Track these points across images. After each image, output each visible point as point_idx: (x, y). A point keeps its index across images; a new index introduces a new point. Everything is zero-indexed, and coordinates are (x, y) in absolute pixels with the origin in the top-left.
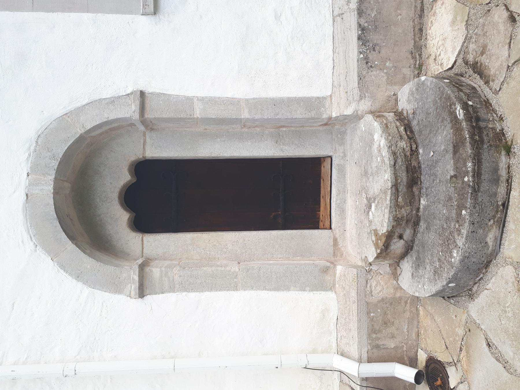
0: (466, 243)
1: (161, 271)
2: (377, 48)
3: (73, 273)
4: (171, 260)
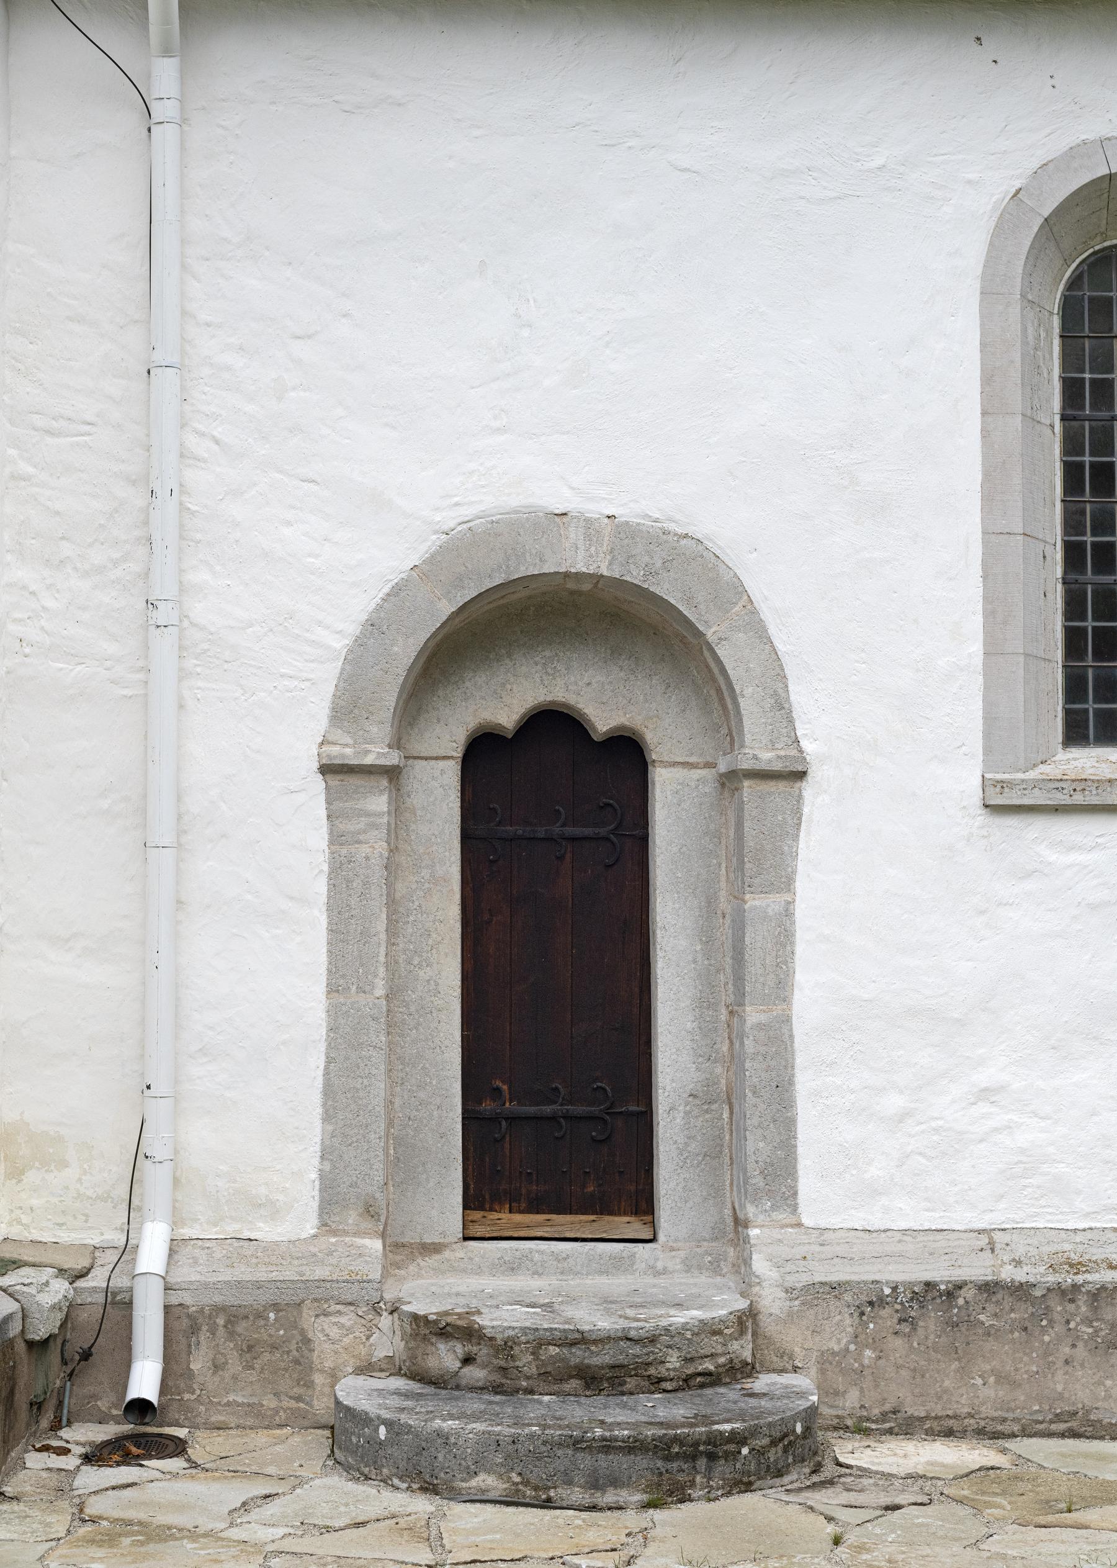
1: (380, 815)
2: (906, 1328)
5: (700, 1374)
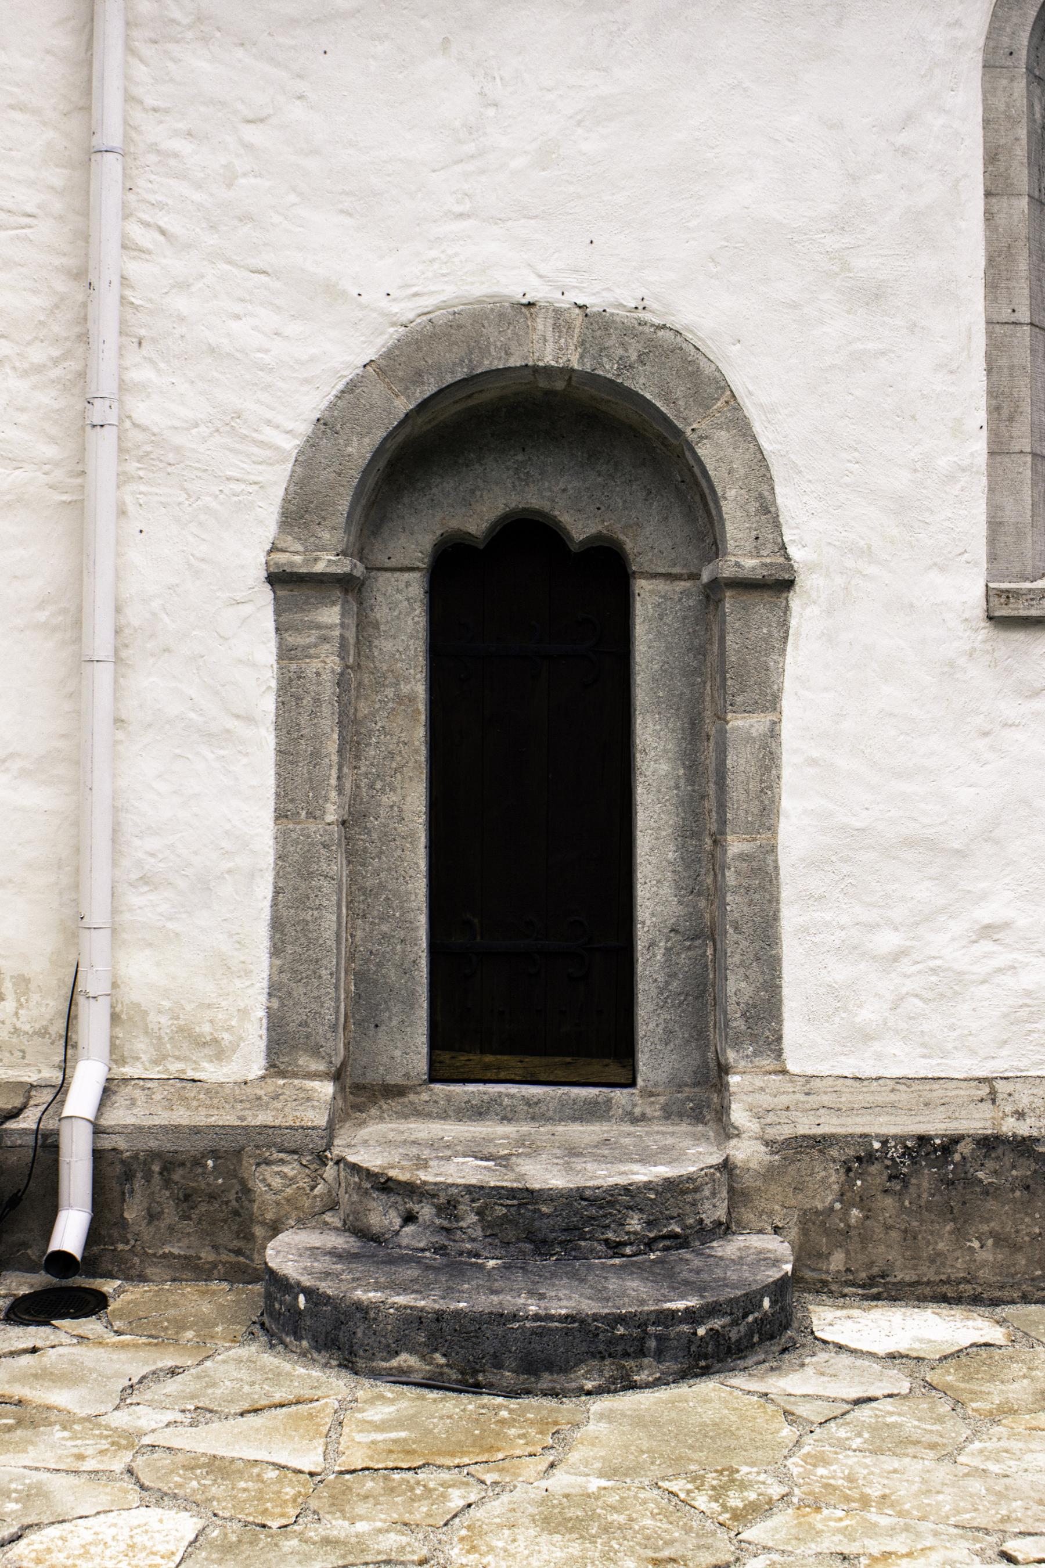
0: (397, 1309)
1: (331, 627)
3: (336, 413)
4: (358, 642)
5: (664, 1237)
